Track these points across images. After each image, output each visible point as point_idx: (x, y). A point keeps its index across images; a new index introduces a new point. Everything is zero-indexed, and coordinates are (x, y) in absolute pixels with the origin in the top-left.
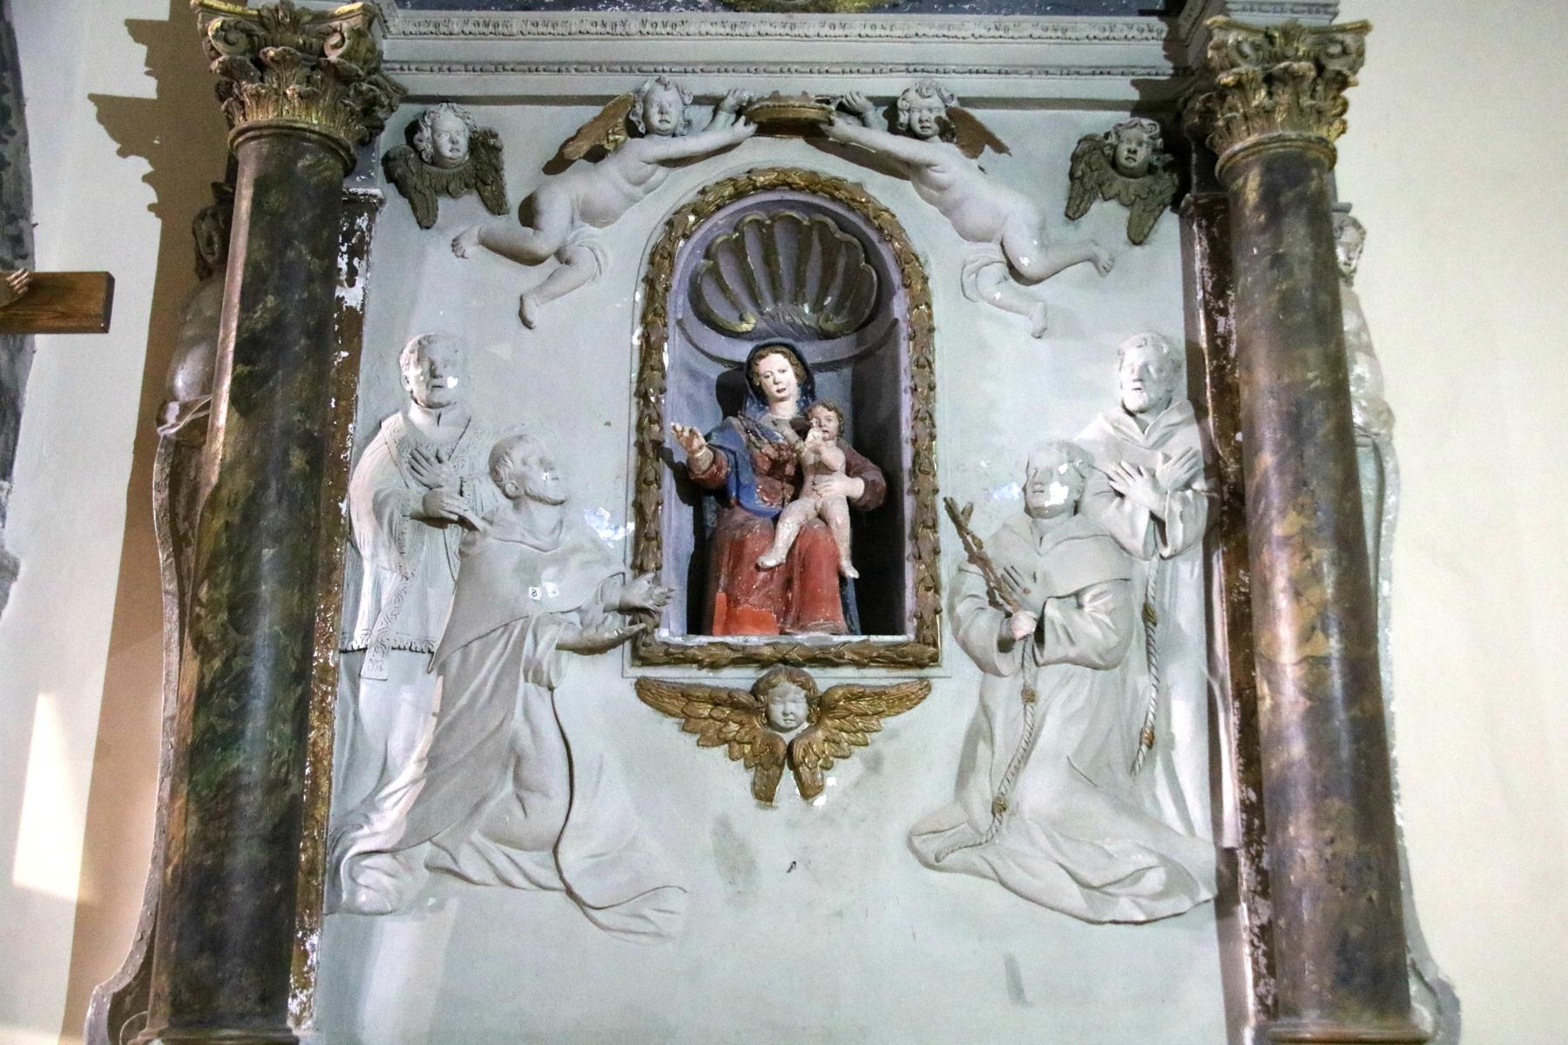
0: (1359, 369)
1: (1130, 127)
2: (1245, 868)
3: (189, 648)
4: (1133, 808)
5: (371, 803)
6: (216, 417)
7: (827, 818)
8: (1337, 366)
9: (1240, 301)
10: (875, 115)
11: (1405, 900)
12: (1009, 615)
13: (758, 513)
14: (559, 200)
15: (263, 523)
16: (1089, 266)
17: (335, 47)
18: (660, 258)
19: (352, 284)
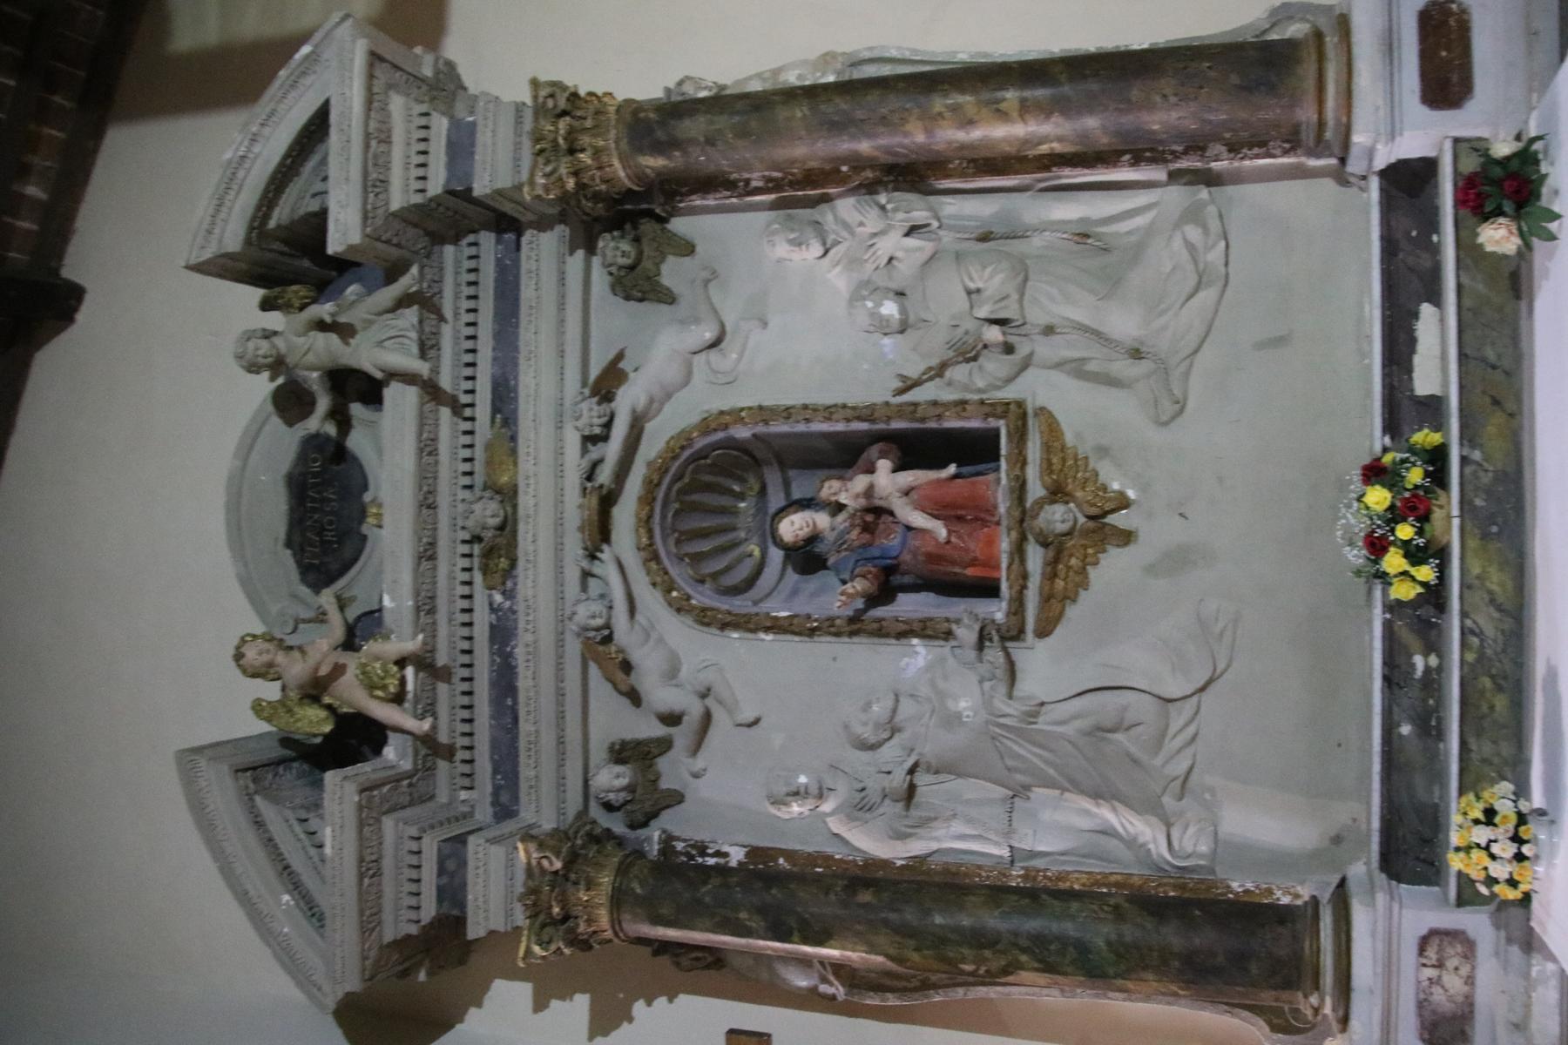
0: (792, 78)
1: (604, 256)
2: (1183, 164)
3: (1010, 979)
4: (1136, 251)
5: (1131, 843)
6: (829, 958)
7: (1144, 489)
8: (791, 95)
9: (740, 169)
10: (595, 452)
11: (1207, 42)
12: (985, 346)
13: (904, 543)
14: (662, 696)
15: (915, 923)
16: (711, 286)
17: (551, 863)
18: (705, 618)
19: (726, 855)
